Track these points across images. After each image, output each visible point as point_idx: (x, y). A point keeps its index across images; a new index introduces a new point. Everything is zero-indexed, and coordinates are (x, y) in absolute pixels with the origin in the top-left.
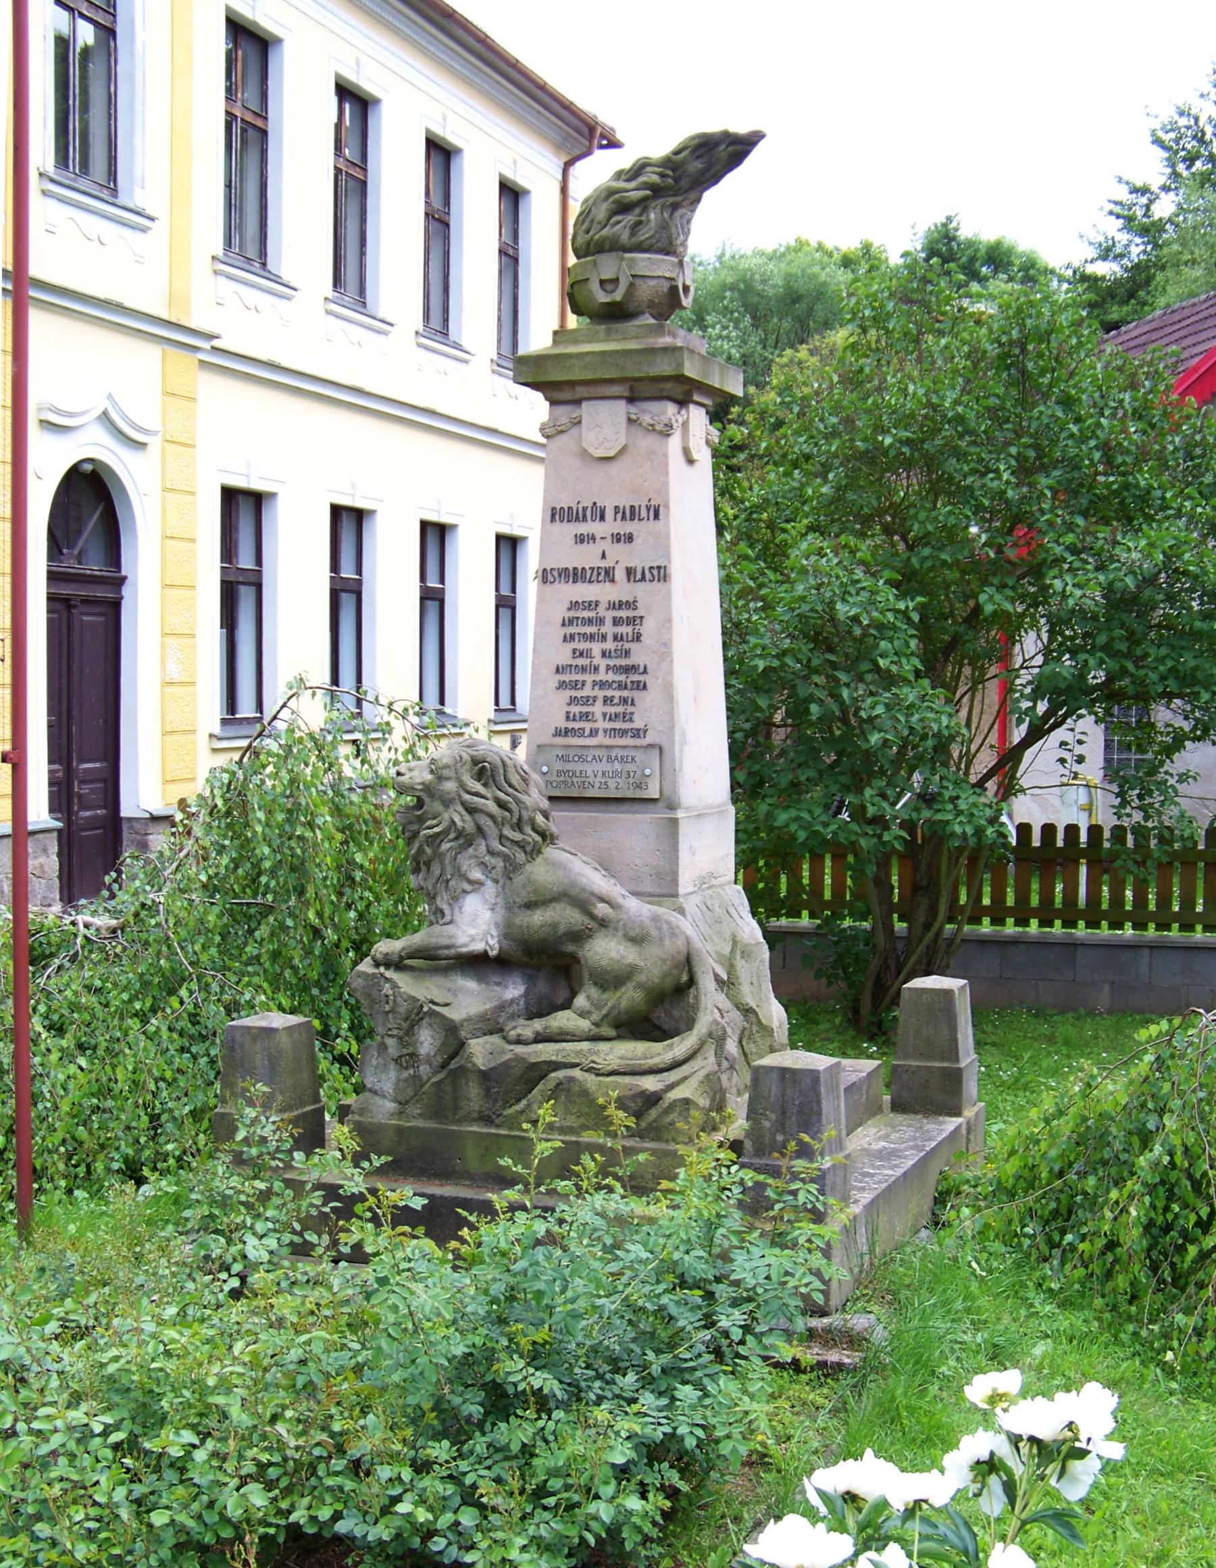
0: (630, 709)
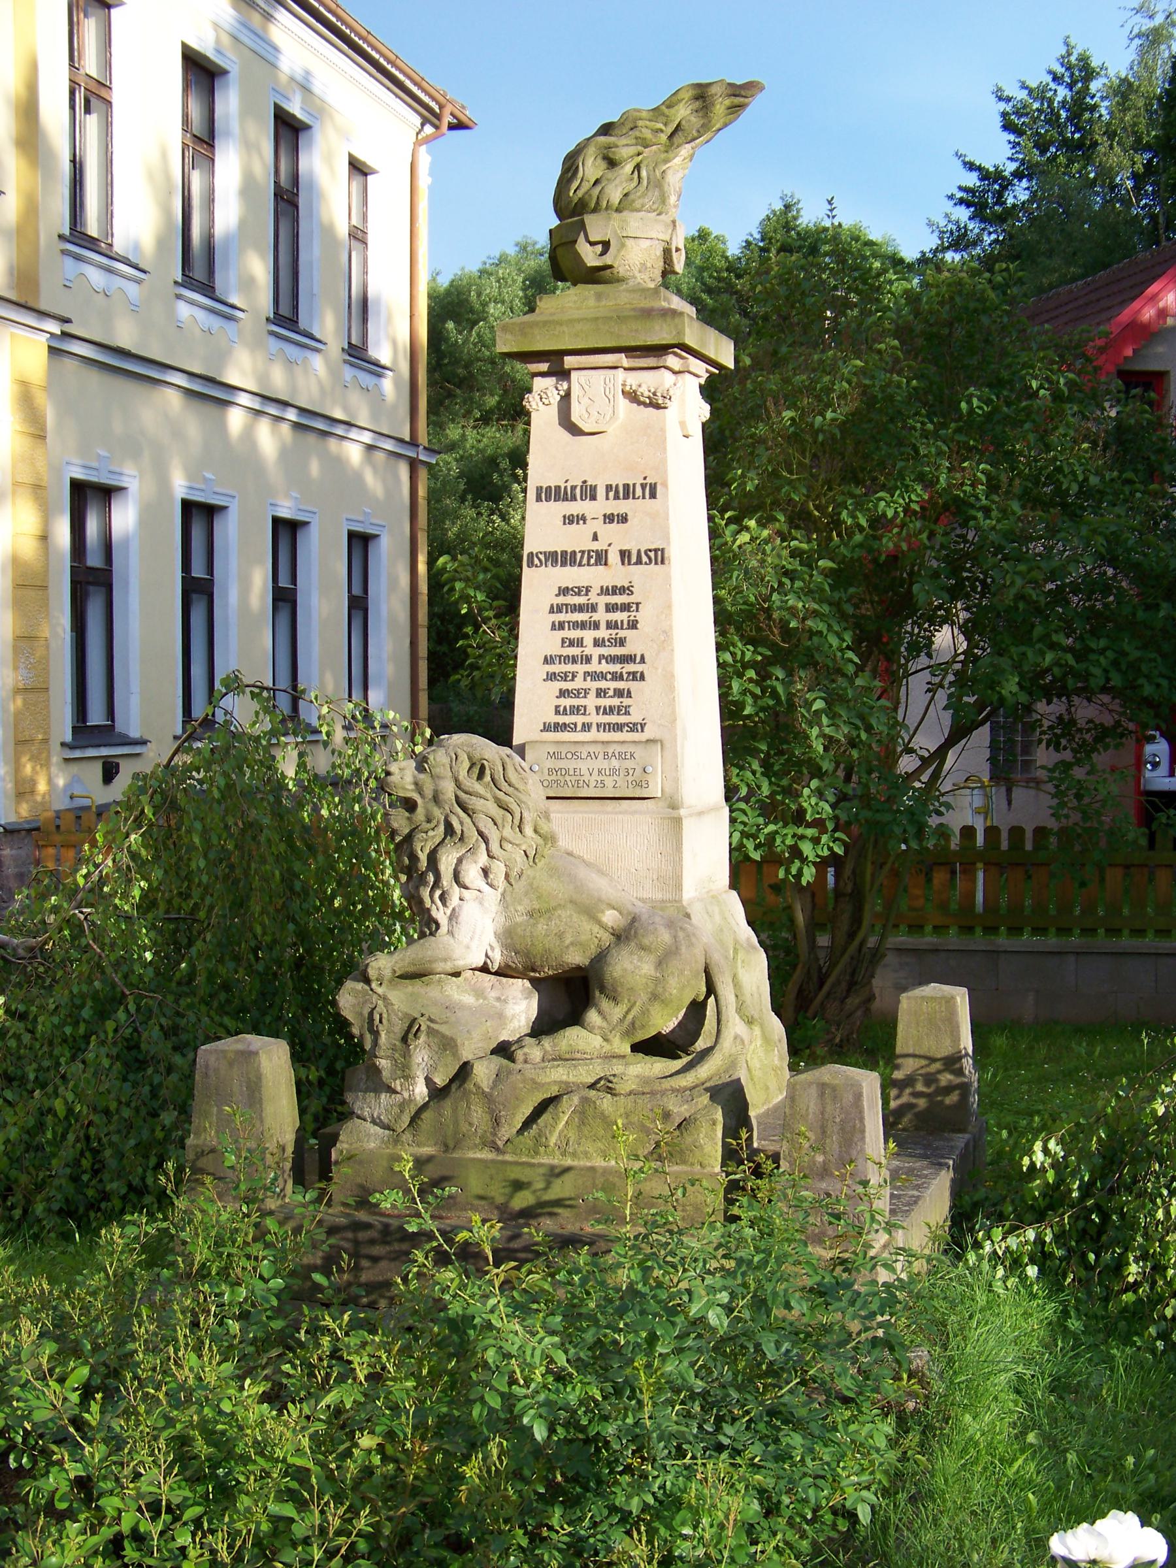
0: (626, 701)
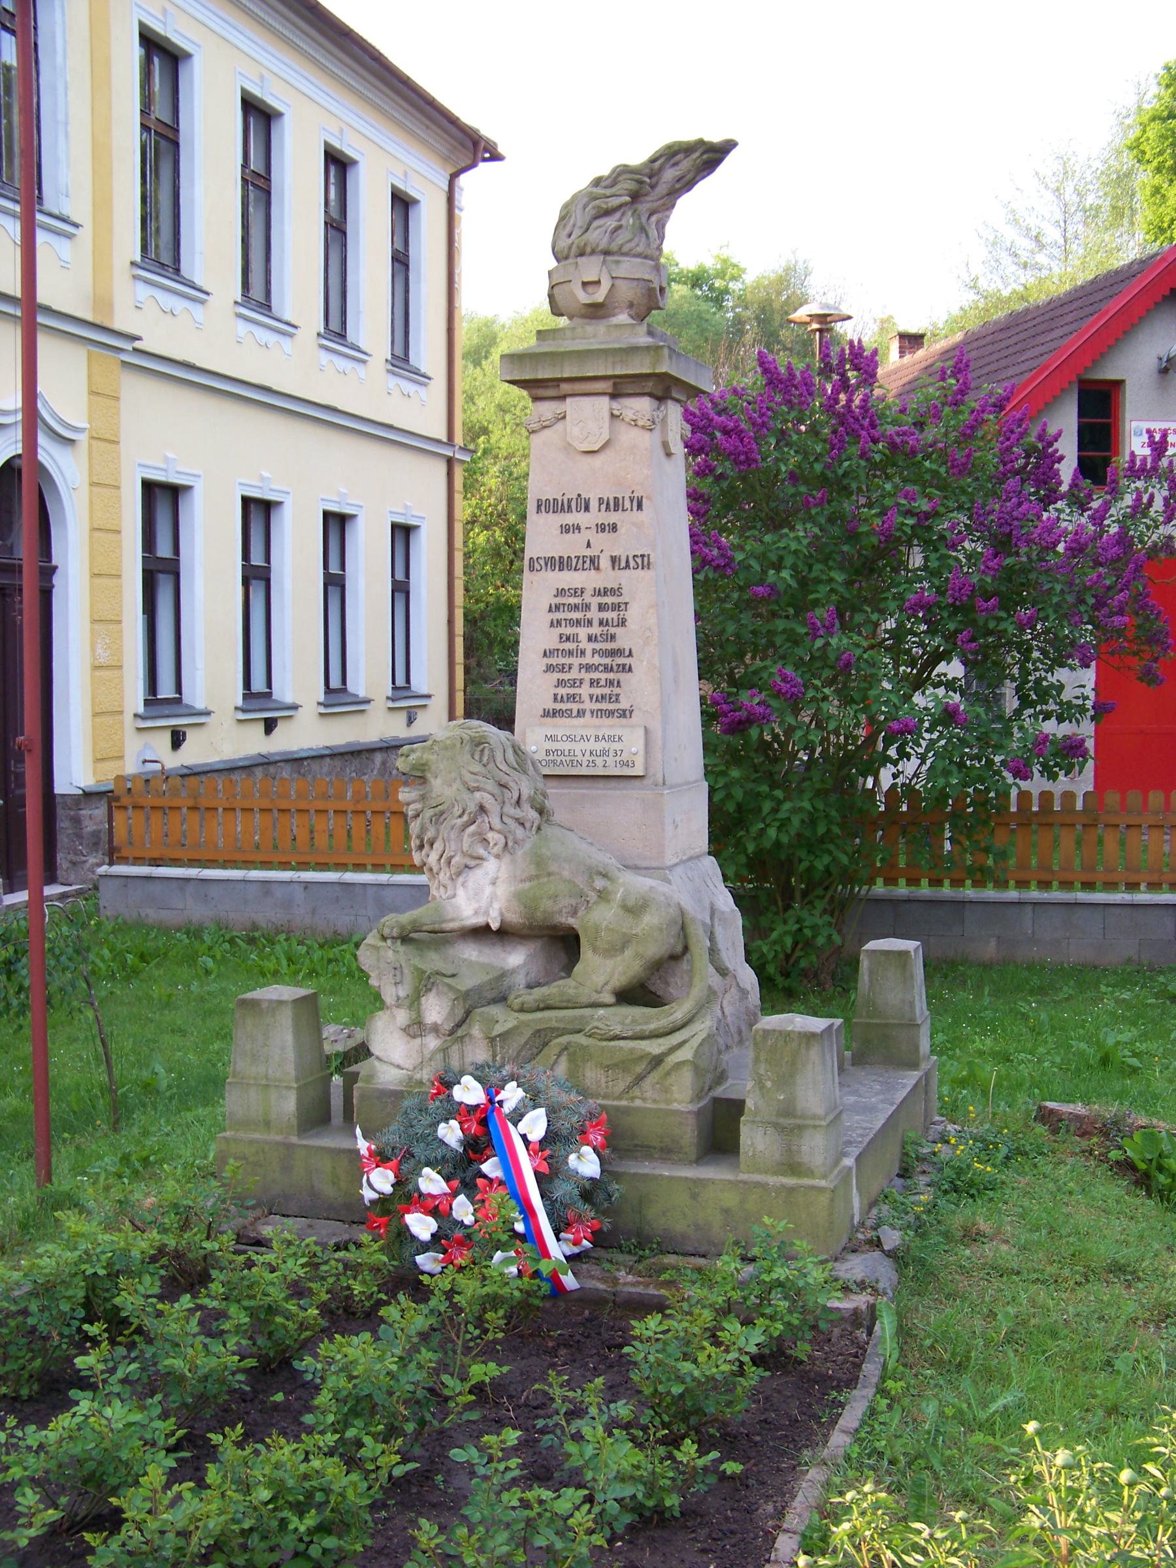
0: (616, 690)
